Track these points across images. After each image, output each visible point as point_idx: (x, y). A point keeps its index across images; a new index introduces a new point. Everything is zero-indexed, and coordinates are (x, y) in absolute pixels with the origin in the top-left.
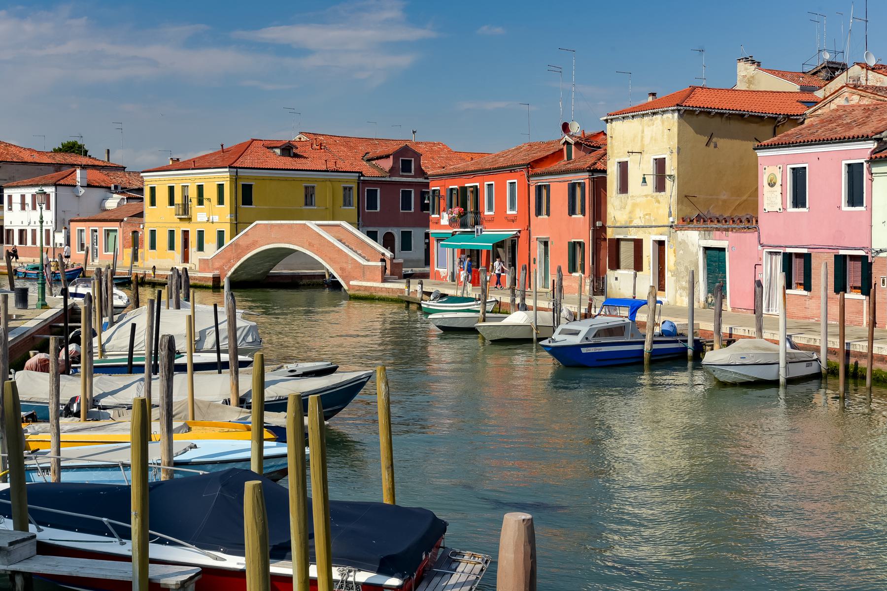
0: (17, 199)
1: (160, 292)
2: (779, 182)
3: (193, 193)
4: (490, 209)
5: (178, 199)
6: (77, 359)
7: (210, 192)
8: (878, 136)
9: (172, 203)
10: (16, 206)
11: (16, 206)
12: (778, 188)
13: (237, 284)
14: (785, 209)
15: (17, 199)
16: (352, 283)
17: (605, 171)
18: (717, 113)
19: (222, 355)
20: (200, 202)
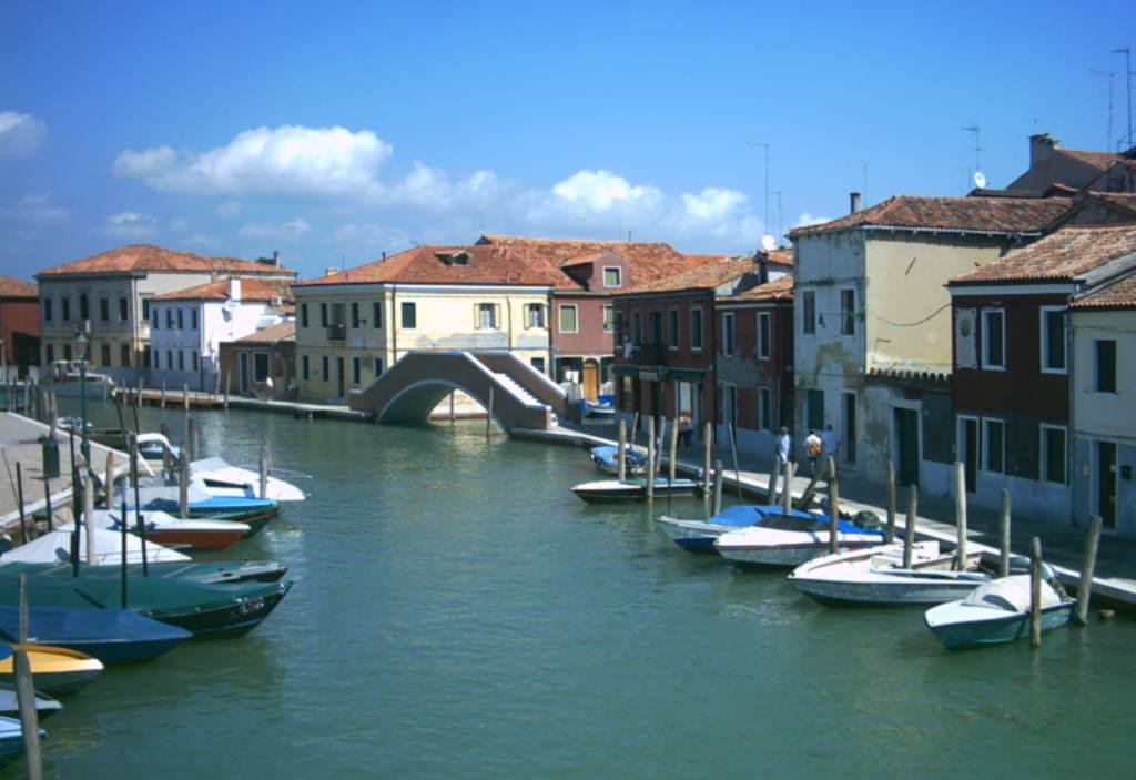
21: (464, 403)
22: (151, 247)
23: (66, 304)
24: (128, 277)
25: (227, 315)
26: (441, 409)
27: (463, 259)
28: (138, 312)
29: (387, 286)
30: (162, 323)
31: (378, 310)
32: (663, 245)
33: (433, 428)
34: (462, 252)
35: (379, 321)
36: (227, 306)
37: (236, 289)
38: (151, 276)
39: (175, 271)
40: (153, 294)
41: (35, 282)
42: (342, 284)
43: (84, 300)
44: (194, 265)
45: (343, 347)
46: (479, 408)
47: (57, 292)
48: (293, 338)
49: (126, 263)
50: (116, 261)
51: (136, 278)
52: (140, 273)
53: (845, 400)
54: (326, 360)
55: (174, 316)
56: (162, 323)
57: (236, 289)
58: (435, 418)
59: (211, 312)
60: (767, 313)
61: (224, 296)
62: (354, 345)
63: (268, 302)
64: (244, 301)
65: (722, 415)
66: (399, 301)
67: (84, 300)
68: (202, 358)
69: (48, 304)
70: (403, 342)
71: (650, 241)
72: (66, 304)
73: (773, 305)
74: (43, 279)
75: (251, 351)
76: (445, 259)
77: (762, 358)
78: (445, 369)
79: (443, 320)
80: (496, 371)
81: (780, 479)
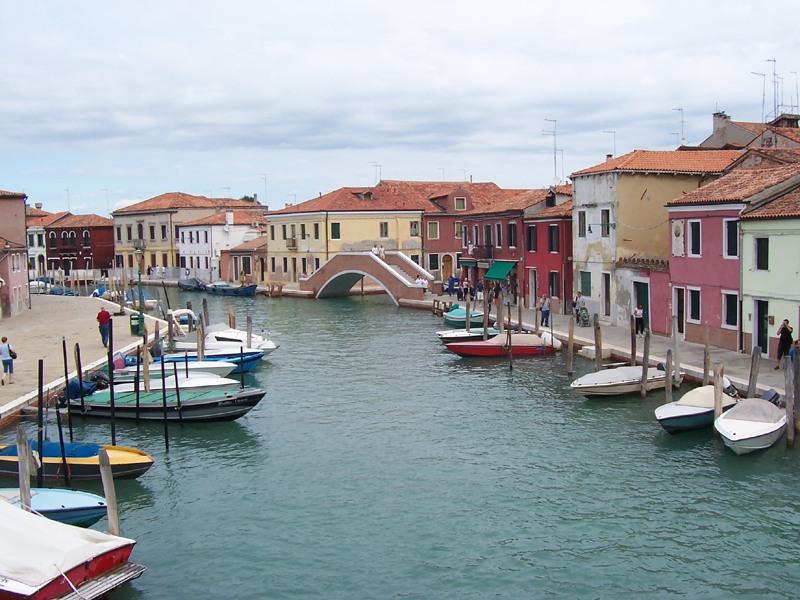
0: (187, 235)
1: (488, 229)
2: (682, 234)
3: (298, 231)
4: (499, 245)
5: (289, 236)
6: (498, 285)
7: (310, 230)
8: (747, 200)
9: (285, 238)
10: (187, 241)
11: (187, 241)
12: (681, 238)
13: (325, 297)
14: (686, 254)
15: (187, 235)
16: (401, 300)
17: (571, 217)
18: (650, 173)
19: (173, 368)
20: (304, 238)
23: (129, 229)
36: (226, 228)
43: (140, 227)
44: (206, 204)
57: (230, 217)
67: (140, 227)
72: (129, 229)
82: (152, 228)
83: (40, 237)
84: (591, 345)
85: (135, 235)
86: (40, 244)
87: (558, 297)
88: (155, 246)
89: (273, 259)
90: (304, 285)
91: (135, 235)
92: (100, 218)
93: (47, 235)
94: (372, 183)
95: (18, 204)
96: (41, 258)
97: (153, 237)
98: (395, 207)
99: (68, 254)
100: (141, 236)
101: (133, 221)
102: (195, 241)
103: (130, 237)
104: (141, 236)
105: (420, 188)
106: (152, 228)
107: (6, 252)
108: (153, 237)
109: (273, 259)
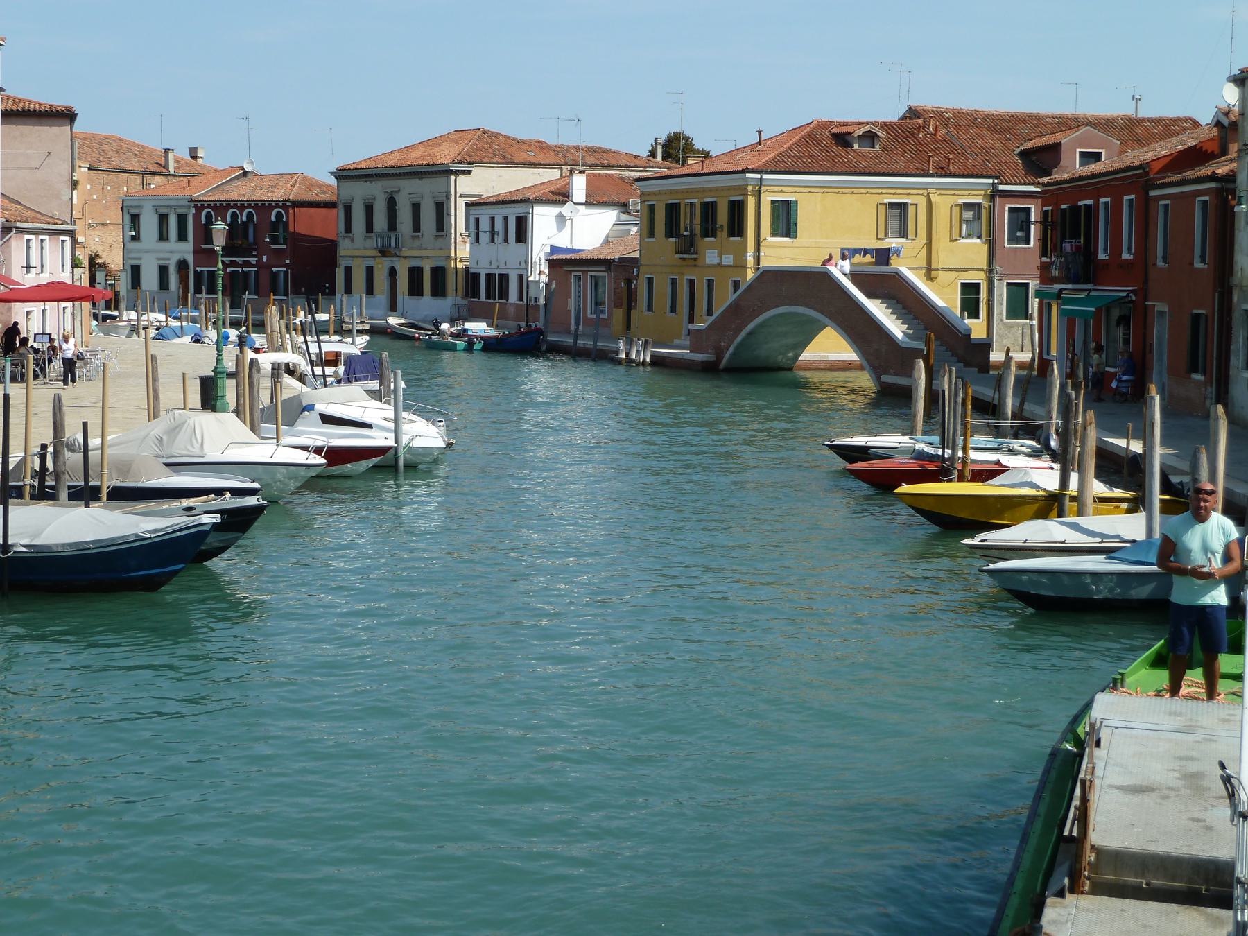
21: (830, 346)
22: (484, 132)
23: (369, 209)
24: (444, 172)
25: (561, 218)
26: (808, 355)
27: (870, 137)
28: (458, 219)
29: (749, 176)
30: (485, 237)
31: (737, 209)
32: (1186, 120)
33: (799, 385)
34: (867, 128)
35: (737, 227)
36: (566, 209)
37: (579, 184)
38: (477, 171)
39: (512, 164)
40: (479, 195)
41: (333, 182)
42: (700, 175)
43: (391, 204)
44: (542, 158)
45: (695, 263)
46: (851, 355)
47: (358, 192)
48: (636, 255)
49: (445, 154)
50: (435, 151)
51: (457, 173)
52: (466, 164)
53: (114, 503)
54: (674, 282)
55: (499, 226)
56: (485, 237)
57: (579, 184)
58: (807, 368)
59: (543, 221)
60: (1207, 198)
61: (561, 196)
62: (708, 262)
63: (624, 207)
64: (588, 204)
65: (1151, 345)
66: (767, 199)
67: (391, 204)
68: (528, 282)
69: (348, 209)
70: (779, 253)
71: (589, 145)
72: (369, 209)
73: (1212, 185)
74: (343, 175)
75: (585, 272)
76: (842, 139)
77: (1198, 265)
78: (812, 291)
79: (830, 228)
80: (870, 295)
81: (1074, 478)
82: (416, 208)
83: (182, 219)
84: (1183, 473)
85: (380, 222)
86: (182, 236)
87: (1204, 374)
88: (420, 248)
89: (650, 281)
90: (697, 341)
91: (380, 222)
92: (309, 183)
93: (197, 217)
94: (893, 114)
95: (57, 134)
96: (182, 265)
97: (416, 227)
98: (845, 169)
99: (239, 260)
100: (392, 225)
101: (377, 191)
102: (499, 239)
103: (369, 227)
104: (392, 225)
105: (1002, 125)
106: (416, 208)
107: (7, 230)
108: (416, 227)
109: (650, 281)
